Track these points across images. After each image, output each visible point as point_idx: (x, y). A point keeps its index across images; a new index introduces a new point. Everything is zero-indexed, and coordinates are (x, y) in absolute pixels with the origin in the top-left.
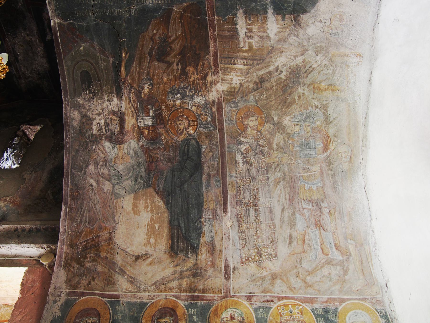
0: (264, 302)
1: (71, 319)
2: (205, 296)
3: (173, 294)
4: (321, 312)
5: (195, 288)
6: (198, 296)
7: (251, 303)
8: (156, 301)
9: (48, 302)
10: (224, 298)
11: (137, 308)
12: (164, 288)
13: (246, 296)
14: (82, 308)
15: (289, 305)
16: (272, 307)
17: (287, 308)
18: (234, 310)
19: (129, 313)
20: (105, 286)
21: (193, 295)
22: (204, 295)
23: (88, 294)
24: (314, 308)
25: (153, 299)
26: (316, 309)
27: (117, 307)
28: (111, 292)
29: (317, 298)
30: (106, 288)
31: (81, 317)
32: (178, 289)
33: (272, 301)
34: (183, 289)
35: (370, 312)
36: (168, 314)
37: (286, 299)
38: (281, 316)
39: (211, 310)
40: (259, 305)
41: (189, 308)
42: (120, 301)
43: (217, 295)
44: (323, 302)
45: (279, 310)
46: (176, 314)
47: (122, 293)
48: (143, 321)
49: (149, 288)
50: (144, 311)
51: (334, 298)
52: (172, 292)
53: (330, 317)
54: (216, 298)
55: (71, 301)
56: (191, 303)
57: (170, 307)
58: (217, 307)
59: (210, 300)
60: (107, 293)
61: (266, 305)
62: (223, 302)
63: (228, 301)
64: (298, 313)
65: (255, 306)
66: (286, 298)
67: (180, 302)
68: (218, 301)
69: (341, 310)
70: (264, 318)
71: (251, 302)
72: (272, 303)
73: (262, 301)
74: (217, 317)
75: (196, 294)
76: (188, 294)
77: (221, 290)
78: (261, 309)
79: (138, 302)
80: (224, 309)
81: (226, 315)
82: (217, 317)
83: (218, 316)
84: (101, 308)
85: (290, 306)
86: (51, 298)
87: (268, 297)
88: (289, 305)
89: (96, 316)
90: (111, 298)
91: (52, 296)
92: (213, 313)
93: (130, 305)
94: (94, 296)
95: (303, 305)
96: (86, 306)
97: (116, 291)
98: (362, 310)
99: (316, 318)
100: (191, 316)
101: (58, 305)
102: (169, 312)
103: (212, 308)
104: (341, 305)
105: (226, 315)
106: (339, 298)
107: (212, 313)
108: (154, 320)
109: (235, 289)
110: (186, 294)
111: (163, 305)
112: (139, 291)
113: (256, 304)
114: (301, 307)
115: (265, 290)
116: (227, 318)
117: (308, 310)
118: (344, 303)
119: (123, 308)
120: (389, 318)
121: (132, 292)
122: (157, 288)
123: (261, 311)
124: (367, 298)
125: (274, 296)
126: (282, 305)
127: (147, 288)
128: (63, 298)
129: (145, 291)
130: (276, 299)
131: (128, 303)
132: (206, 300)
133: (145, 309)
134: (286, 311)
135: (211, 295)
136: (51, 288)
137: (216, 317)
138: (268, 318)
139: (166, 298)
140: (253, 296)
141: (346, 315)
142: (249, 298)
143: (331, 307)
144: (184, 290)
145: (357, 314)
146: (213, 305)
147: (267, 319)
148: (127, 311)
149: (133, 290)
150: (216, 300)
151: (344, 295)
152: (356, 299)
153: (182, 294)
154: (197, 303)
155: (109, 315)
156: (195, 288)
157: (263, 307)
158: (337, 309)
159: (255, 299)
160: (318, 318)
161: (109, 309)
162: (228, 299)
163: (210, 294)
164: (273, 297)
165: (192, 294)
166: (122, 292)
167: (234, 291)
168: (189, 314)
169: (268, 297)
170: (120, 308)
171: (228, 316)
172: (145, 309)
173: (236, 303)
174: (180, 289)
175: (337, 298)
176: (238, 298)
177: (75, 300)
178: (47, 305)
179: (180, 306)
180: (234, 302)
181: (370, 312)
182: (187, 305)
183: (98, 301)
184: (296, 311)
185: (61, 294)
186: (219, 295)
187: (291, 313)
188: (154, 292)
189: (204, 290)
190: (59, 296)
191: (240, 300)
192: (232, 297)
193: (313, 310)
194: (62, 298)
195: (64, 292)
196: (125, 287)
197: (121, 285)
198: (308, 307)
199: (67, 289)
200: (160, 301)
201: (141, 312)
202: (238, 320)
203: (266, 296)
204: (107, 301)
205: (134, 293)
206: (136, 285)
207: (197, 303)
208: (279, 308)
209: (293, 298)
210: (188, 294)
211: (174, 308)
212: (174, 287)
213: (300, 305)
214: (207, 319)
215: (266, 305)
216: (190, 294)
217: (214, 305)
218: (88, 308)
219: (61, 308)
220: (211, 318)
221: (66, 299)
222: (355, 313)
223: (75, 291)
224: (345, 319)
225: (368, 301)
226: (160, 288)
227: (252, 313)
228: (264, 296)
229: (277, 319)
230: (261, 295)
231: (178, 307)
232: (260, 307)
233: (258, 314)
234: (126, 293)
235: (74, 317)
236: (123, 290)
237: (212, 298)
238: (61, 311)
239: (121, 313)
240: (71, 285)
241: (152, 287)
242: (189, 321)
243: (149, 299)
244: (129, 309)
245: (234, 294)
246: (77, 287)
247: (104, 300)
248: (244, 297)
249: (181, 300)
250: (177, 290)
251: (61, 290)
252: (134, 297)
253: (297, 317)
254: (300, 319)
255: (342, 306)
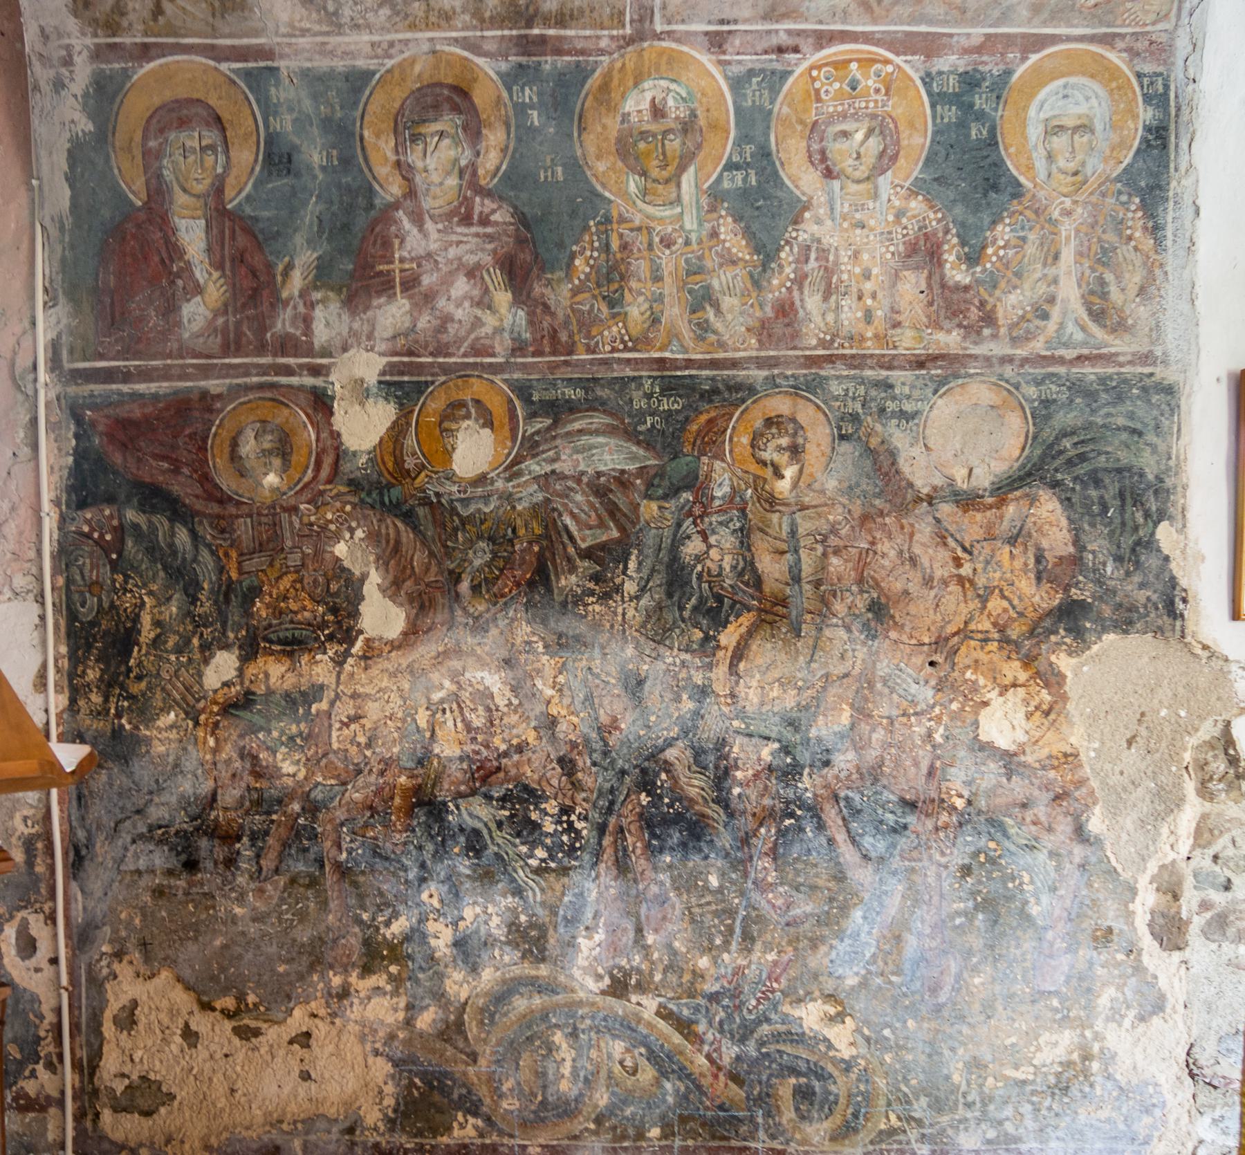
0: (766, 52)
1: (131, 140)
2: (565, 38)
3: (454, 34)
4: (952, 85)
5: (531, 10)
6: (543, 40)
7: (723, 57)
8: (400, 65)
9: (36, 88)
10: (630, 41)
11: (338, 90)
12: (421, 14)
13: (707, 33)
14: (157, 101)
15: (850, 61)
16: (790, 73)
17: (841, 73)
18: (663, 83)
19: (317, 108)
20: (214, 15)
21: (526, 36)
22: (562, 32)
23: (164, 50)
24: (934, 70)
25: (390, 57)
26: (940, 73)
27: (273, 91)
28: (241, 37)
29: (951, 35)
30: (218, 23)
31: (161, 131)
32: (474, 15)
33: (796, 50)
34: (487, 14)
35: (1114, 85)
36: (446, 106)
37: (843, 42)
38: (819, 100)
39: (587, 86)
40: (750, 66)
41: (515, 82)
42: (277, 69)
43: (606, 32)
44: (966, 51)
45: (814, 80)
46: (472, 104)
47: (279, 40)
48: (366, 133)
49: (370, 15)
50: (364, 99)
51: (1008, 36)
52: (452, 28)
53: (978, 102)
54: (603, 43)
55: (111, 77)
56: (520, 66)
57: (450, 81)
58: (607, 77)
59: (582, 52)
60: (228, 42)
61: (772, 62)
62: (627, 57)
63: (646, 55)
64: (877, 91)
65: (735, 70)
66: (845, 37)
67: (481, 61)
68: (611, 54)
69: (1021, 77)
70: (761, 109)
71: (724, 53)
72: (793, 56)
73: (759, 49)
74: (609, 110)
75: (536, 31)
76: (506, 32)
77: (622, 13)
78: (754, 80)
79: (341, 69)
80: (631, 83)
81: (638, 103)
82: (609, 110)
83: (612, 108)
84: (220, 98)
85: (854, 66)
86: (40, 73)
87: (782, 34)
88: (850, 61)
89: (208, 124)
90: (246, 61)
91: (44, 65)
92: (596, 99)
93: (316, 81)
94: (185, 57)
95: (899, 60)
96: (168, 95)
97: (256, 33)
98: (1092, 76)
99: (933, 106)
100: (521, 109)
101: (75, 96)
102: (449, 99)
103: (590, 81)
104: (1024, 59)
105: (638, 103)
106: (1024, 36)
107: (590, 97)
108: (400, 127)
109: (671, 9)
110: (499, 33)
111: (426, 76)
112: (338, 29)
113: (740, 62)
114: (890, 68)
115: (773, 10)
116: (640, 111)
117: (912, 80)
118: (1038, 51)
119: (292, 94)
120: (1172, 103)
121: (315, 35)
122: (398, 14)
123: (755, 87)
124: (1119, 35)
125: (804, 31)
126: (826, 65)
127: (364, 18)
128: (82, 74)
129: (357, 26)
130: (810, 40)
131: (305, 73)
132: (569, 53)
133: (367, 93)
134: (837, 85)
135: (588, 33)
136: (30, 36)
137: (603, 110)
138: (776, 110)
139: (434, 52)
140: (730, 32)
141: (1032, 96)
142: (717, 42)
143: (991, 66)
144: (492, 18)
145: (1069, 91)
146: (594, 71)
147: (770, 112)
148: (307, 104)
149: (317, 28)
150: (602, 52)
151: (1044, 23)
152: (1081, 39)
153: (486, 33)
154: (539, 63)
155: (250, 121)
156: (531, 10)
157: (762, 70)
158: (1008, 73)
159: (737, 42)
160: (939, 108)
161: (247, 98)
162: (646, 44)
163: (584, 28)
164: (799, 33)
165: (523, 32)
166: (277, 34)
167: (668, 14)
168: (515, 105)
169: (782, 34)
170: (283, 95)
171: (645, 105)
172: (367, 93)
173: (673, 59)
174: (477, 14)
175: (1015, 36)
176: (678, 41)
177: (126, 74)
178: (35, 100)
179: (481, 76)
180: (665, 58)
181: (1114, 85)
182: (508, 74)
183: (205, 71)
184: (870, 83)
185: (70, 56)
186: (615, 32)
187: (854, 89)
188: (389, 31)
189: (563, 14)
190: (68, 62)
191: (685, 49)
192: (658, 37)
193: (927, 79)
194: (77, 69)
195: (78, 48)
196: (284, 17)
197: (270, 11)
198: (910, 66)
199: (84, 34)
200: (413, 61)
201: (356, 103)
202: (677, 118)
203: (777, 31)
204: (233, 71)
205: (319, 39)
206: (325, 8)
207: (539, 63)
208: (815, 73)
209: (867, 38)
210: (506, 32)
211: (463, 86)
212: (458, 10)
213: (887, 62)
214: (725, 28)
215: (772, 62)
216: (514, 32)
217: (599, 71)
218: (177, 101)
219: (85, 105)
220: (589, 115)
221: (94, 73)
222: (1065, 87)
223: (117, 40)
224: (1026, 108)
225: (1120, 44)
226: (407, 16)
227: (722, 95)
228: (769, 32)
229: (806, 111)
230: (759, 27)
231: (475, 80)
232: (751, 73)
233: (745, 95)
234: (293, 40)
235: (139, 134)
236: (283, 30)
237: (589, 45)
238: (91, 117)
239: (291, 110)
240: (96, 21)
241: (381, 12)
242: (518, 127)
243: (377, 57)
244: (315, 97)
245: (667, 28)
246: (118, 24)
247: (224, 67)
248: (701, 38)
249: (485, 54)
250: (467, 17)
251: (67, 41)
252: (323, 50)
253: (872, 105)
254: (879, 111)
255: (1029, 63)
